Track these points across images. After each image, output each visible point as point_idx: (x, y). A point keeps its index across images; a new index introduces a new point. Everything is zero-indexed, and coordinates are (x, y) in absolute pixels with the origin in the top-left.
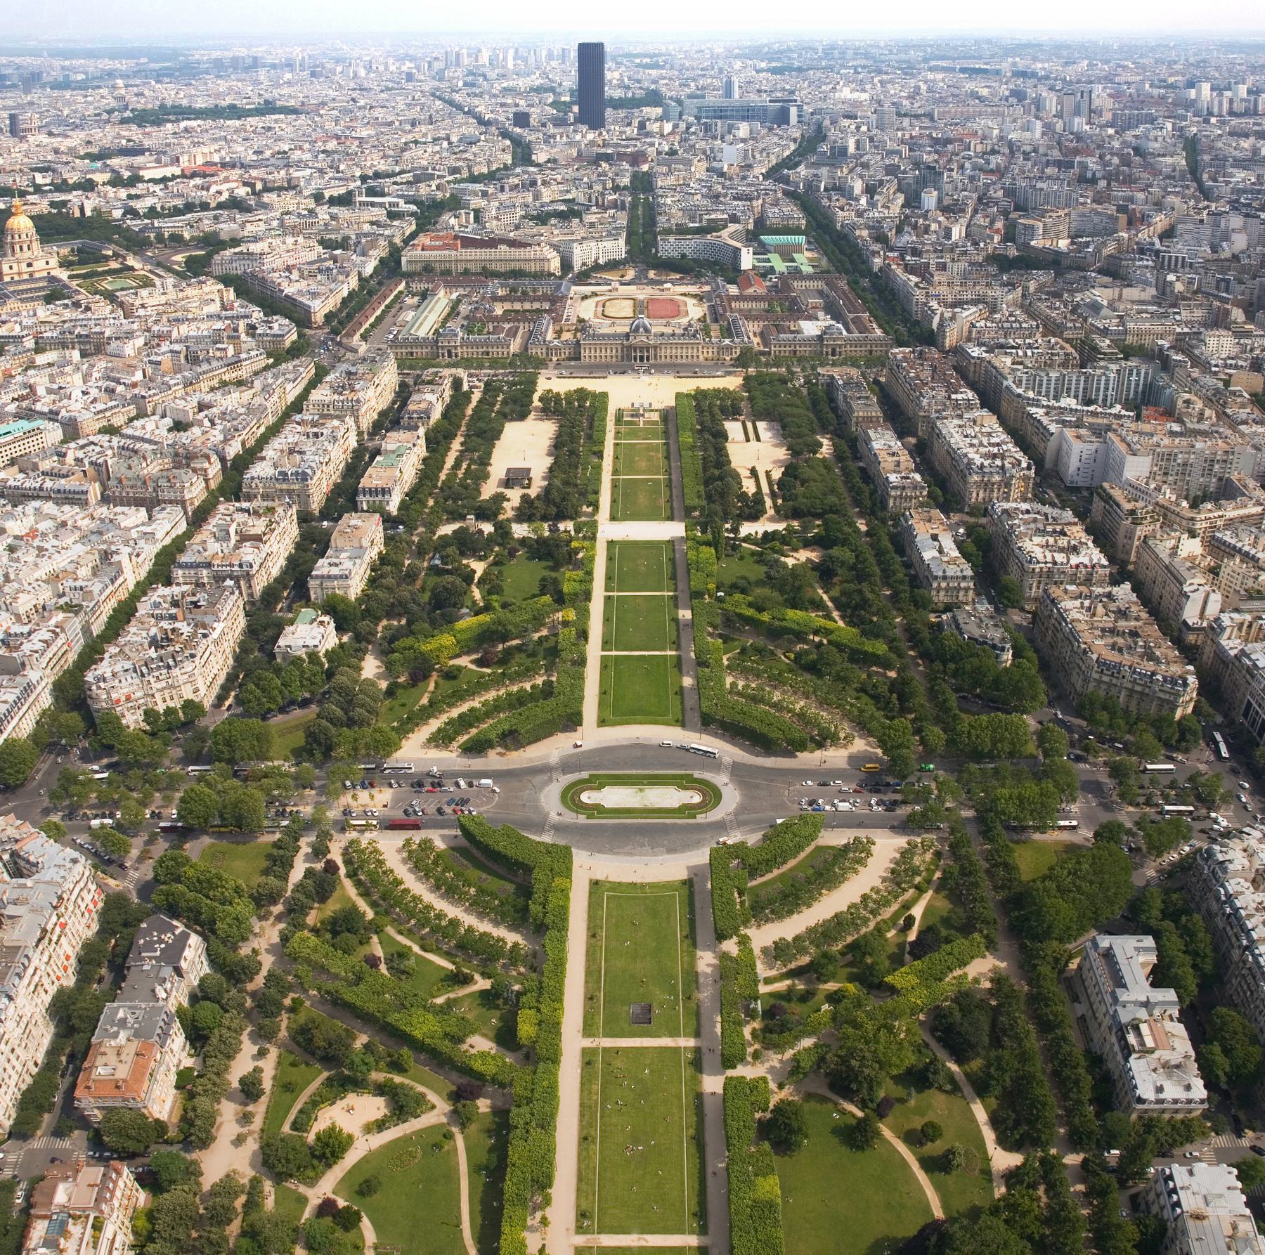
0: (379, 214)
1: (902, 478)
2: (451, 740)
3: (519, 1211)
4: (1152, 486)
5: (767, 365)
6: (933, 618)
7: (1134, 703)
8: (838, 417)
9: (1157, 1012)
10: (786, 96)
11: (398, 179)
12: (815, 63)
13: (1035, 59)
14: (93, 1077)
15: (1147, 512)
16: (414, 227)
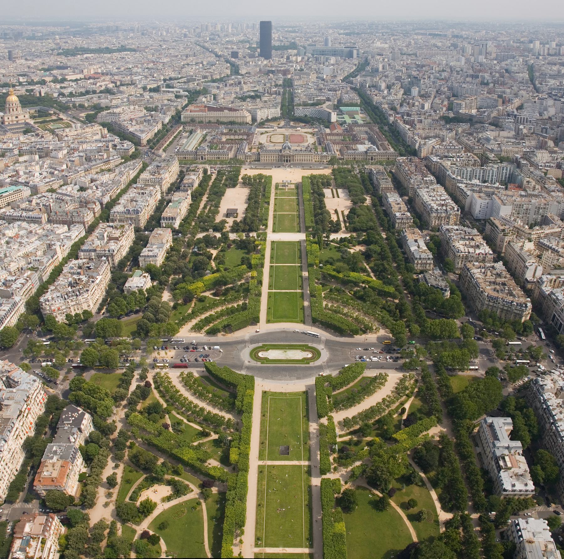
1: (402, 214)
4: (512, 219)
7: (503, 315)
8: (374, 187)
9: (512, 451)
10: (352, 46)
11: (180, 81)
13: (462, 30)
16: (187, 102)
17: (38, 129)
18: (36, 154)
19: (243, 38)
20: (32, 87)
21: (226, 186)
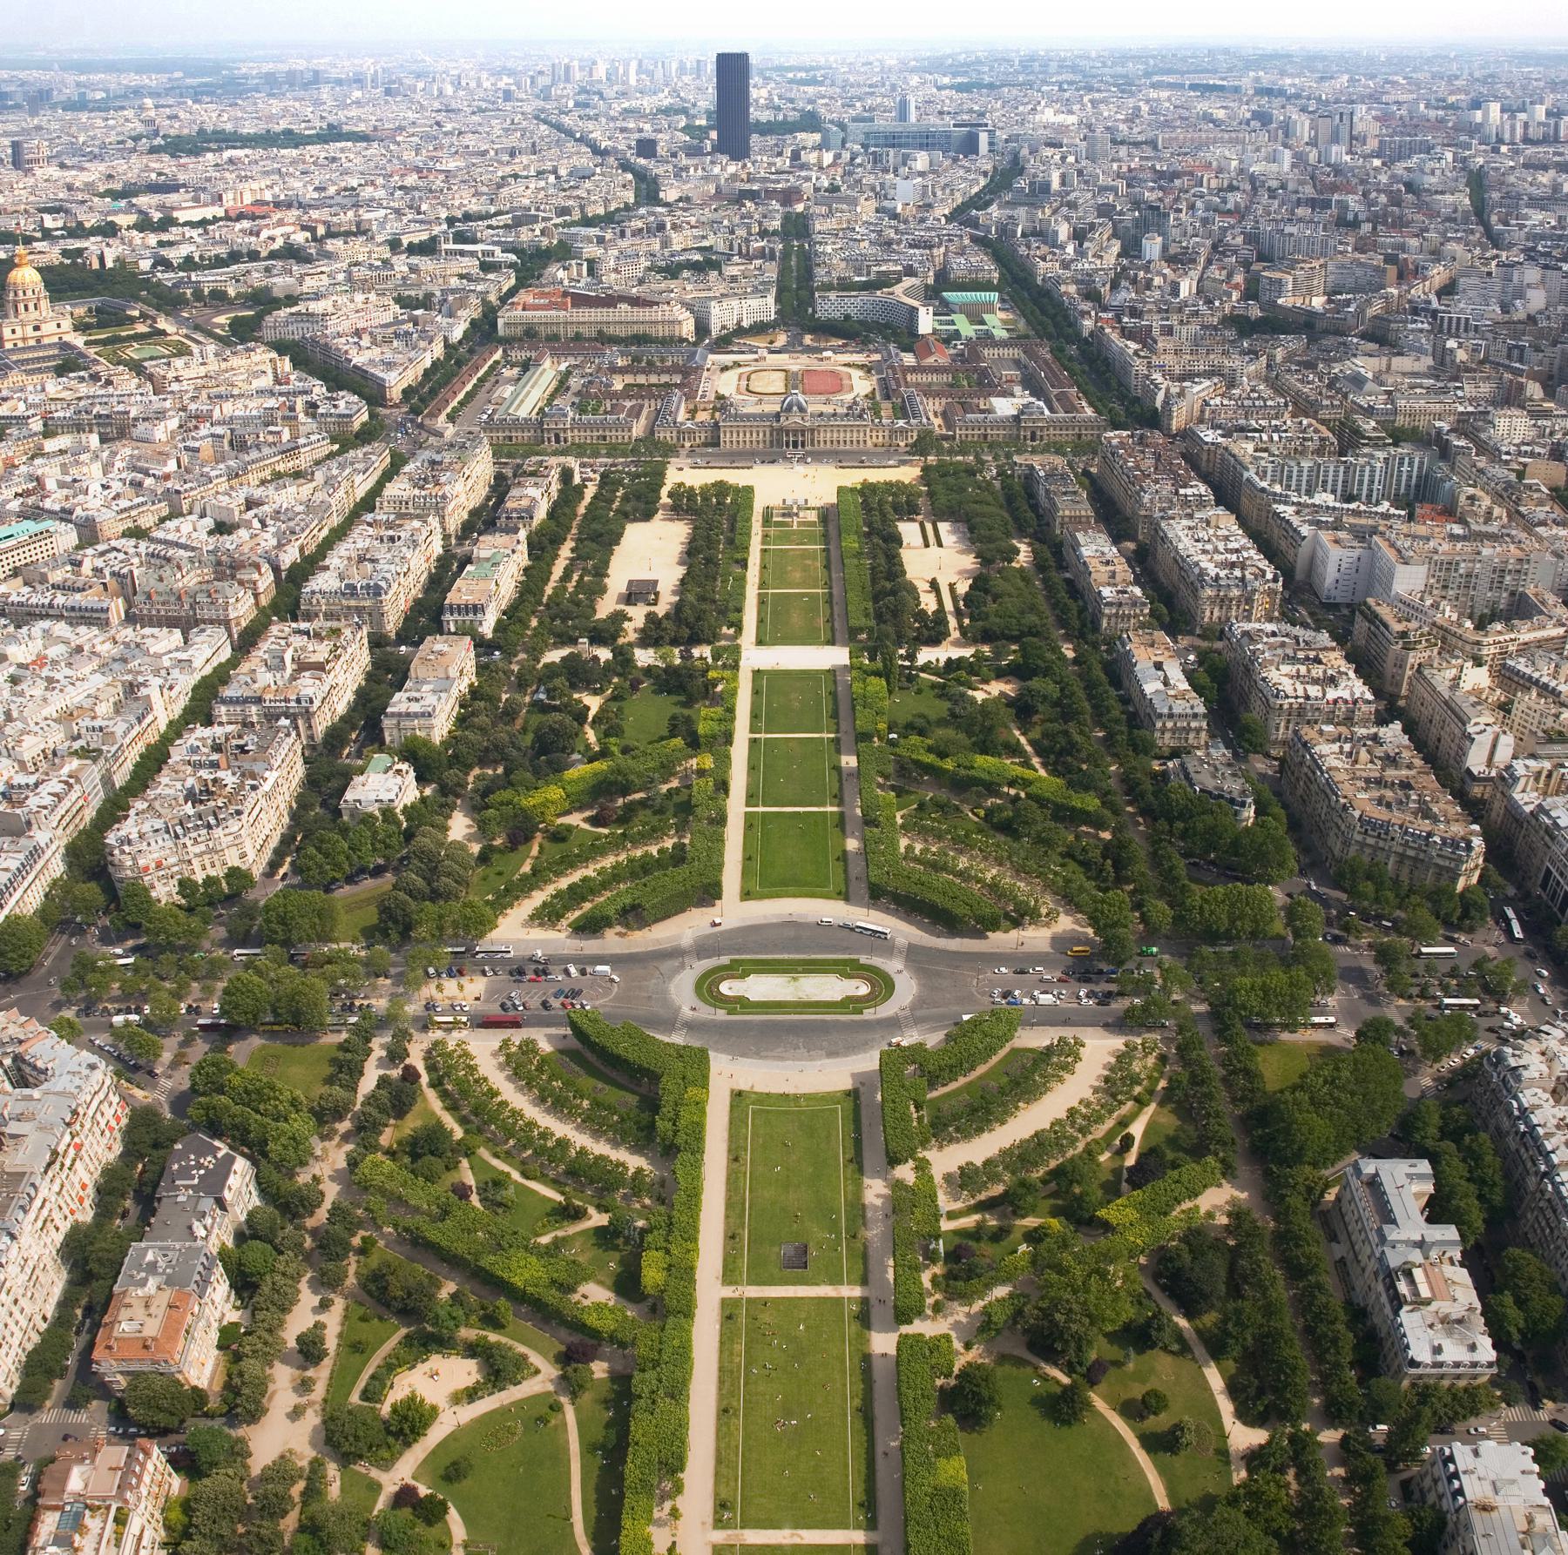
0: (470, 265)
1: (1119, 592)
2: (560, 916)
3: (643, 1501)
4: (1428, 602)
5: (951, 452)
6: (1156, 766)
7: (1405, 871)
8: (1039, 517)
9: (1434, 1254)
10: (974, 119)
11: (493, 222)
12: (1010, 78)
13: (1283, 73)
15: (1422, 635)
16: (513, 281)
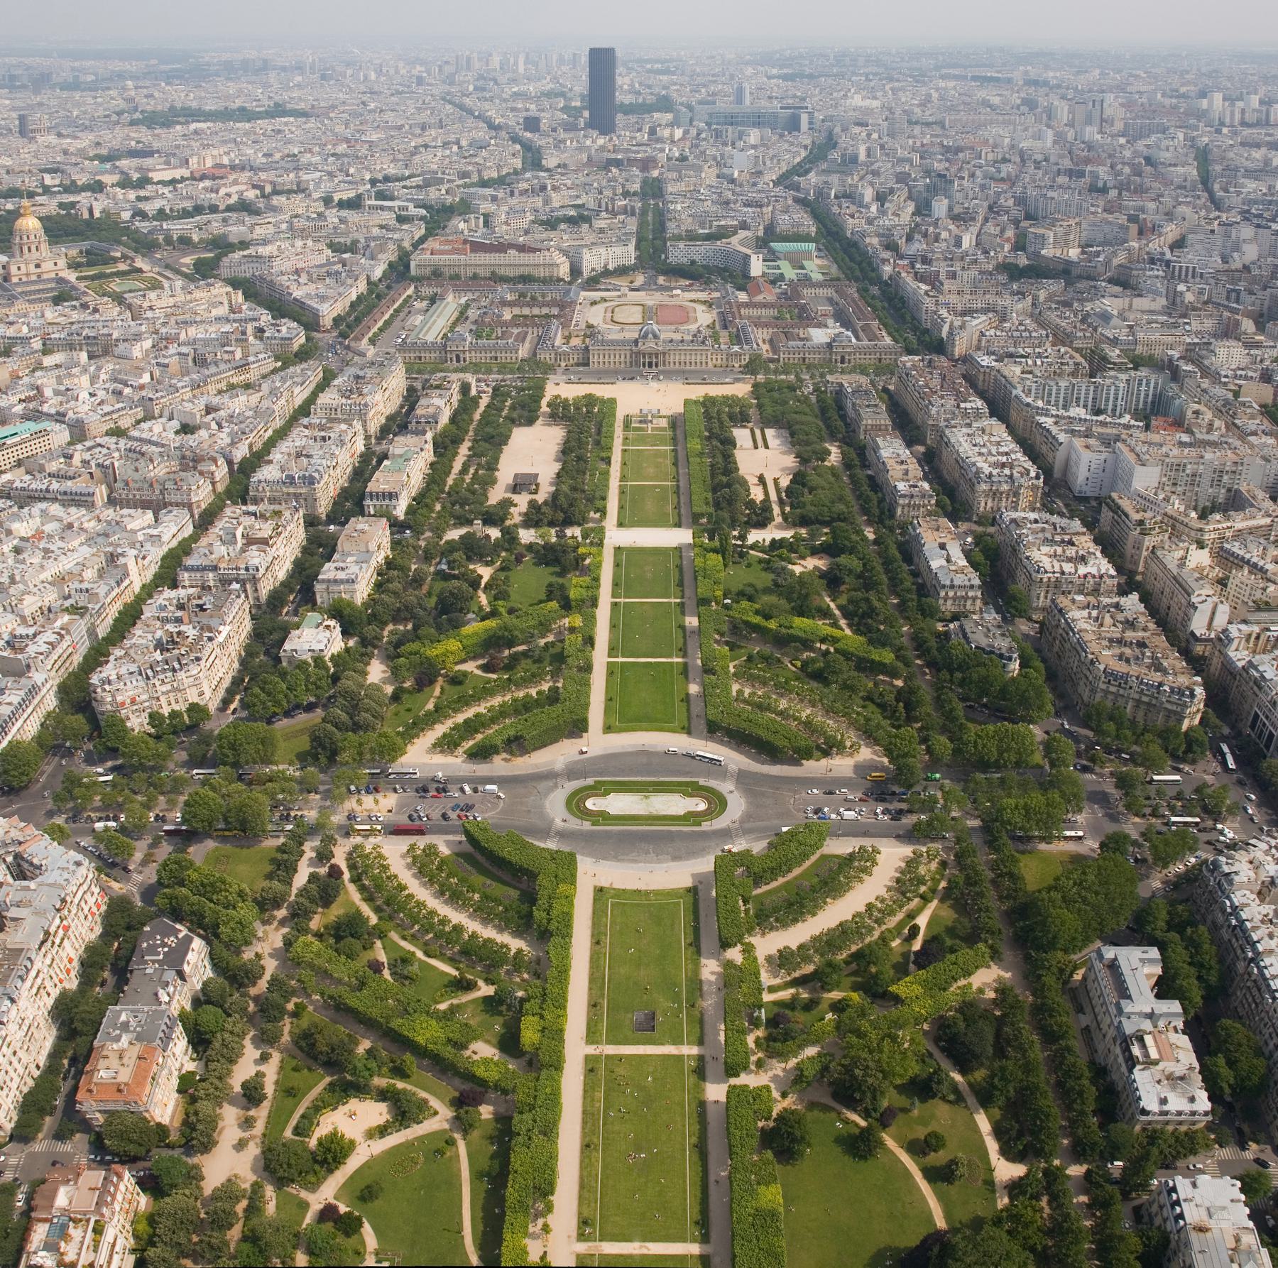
1: (911, 486)
4: (1161, 497)
7: (1140, 714)
8: (847, 425)
9: (1161, 1024)
10: (797, 103)
11: (408, 183)
13: (1047, 68)
14: (95, 1080)
16: (423, 231)
17: (85, 294)
18: (81, 350)
19: (551, 86)
20: (72, 198)
21: (513, 421)
